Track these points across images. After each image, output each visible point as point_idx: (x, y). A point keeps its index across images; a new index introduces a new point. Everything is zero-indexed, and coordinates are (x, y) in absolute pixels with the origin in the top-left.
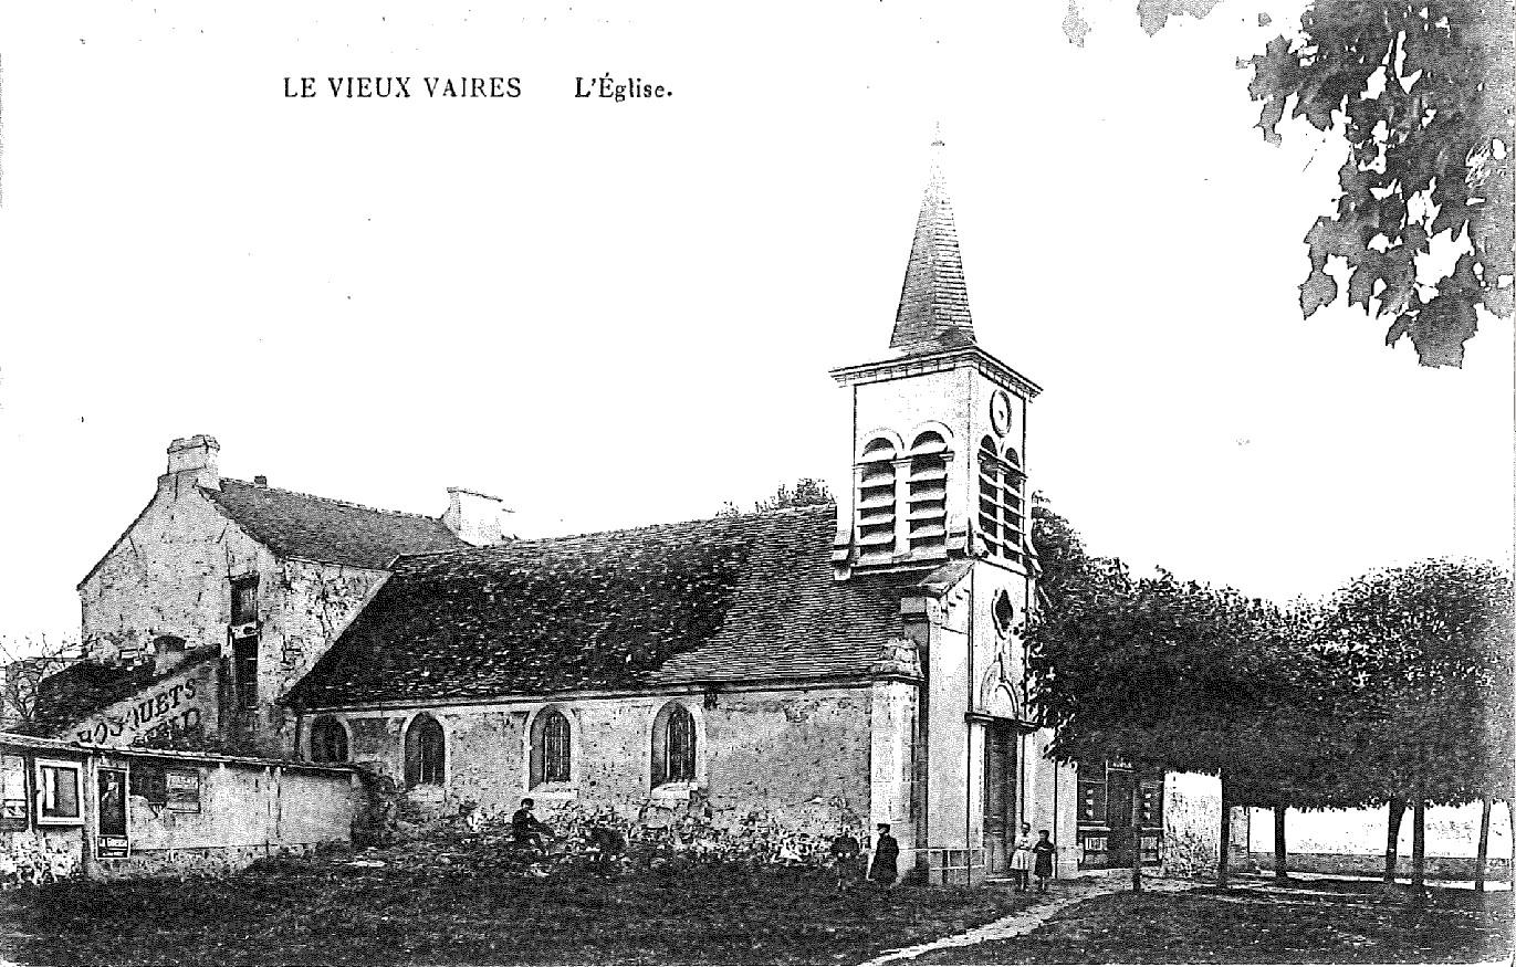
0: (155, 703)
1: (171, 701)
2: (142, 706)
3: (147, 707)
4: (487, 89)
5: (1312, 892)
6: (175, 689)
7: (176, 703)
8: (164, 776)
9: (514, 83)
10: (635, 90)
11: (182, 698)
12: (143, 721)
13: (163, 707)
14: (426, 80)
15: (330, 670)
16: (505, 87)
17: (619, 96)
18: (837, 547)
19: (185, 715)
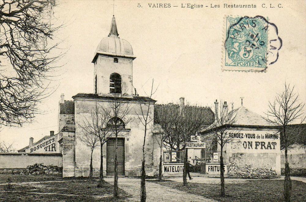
0: (46, 143)
1: (49, 142)
2: (43, 144)
3: (44, 144)
4: (163, 6)
5: (31, 193)
6: (50, 140)
7: (50, 143)
8: (288, 125)
9: (169, 5)
10: (196, 6)
11: (51, 141)
12: (43, 146)
13: (47, 144)
14: (149, 4)
15: (297, 127)
16: (167, 6)
17: (192, 8)
18: (22, 7)
19: (52, 145)
